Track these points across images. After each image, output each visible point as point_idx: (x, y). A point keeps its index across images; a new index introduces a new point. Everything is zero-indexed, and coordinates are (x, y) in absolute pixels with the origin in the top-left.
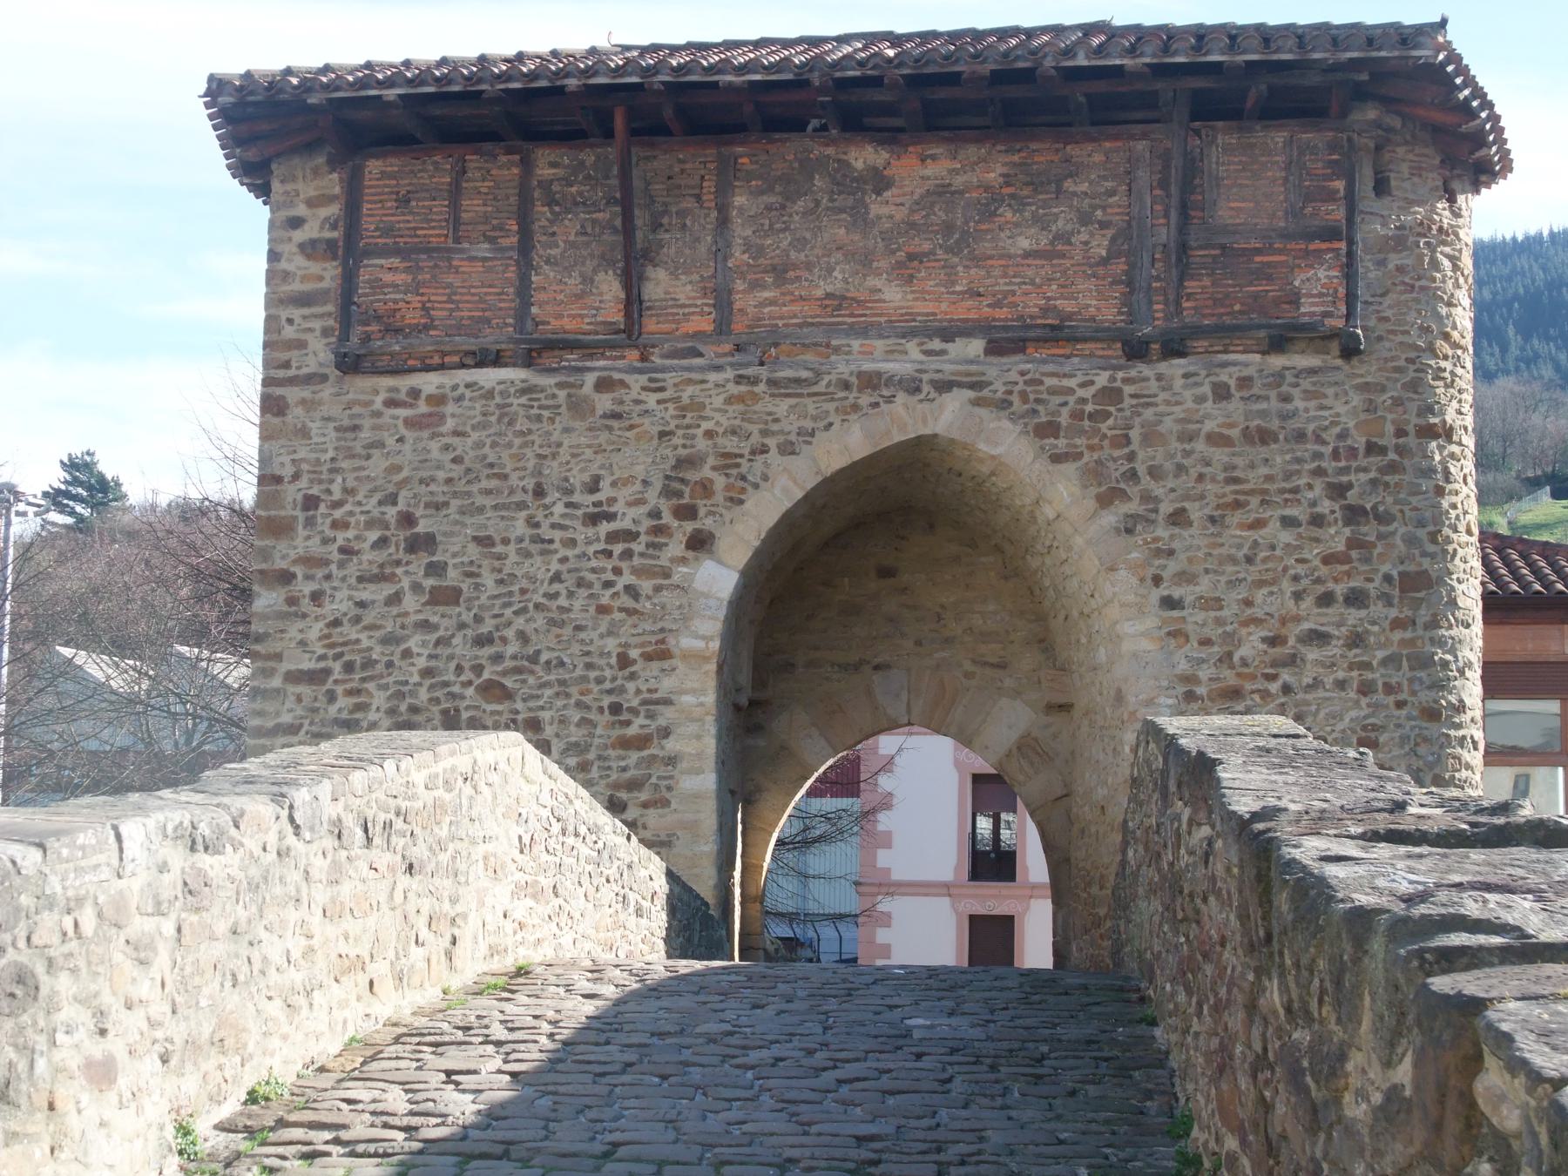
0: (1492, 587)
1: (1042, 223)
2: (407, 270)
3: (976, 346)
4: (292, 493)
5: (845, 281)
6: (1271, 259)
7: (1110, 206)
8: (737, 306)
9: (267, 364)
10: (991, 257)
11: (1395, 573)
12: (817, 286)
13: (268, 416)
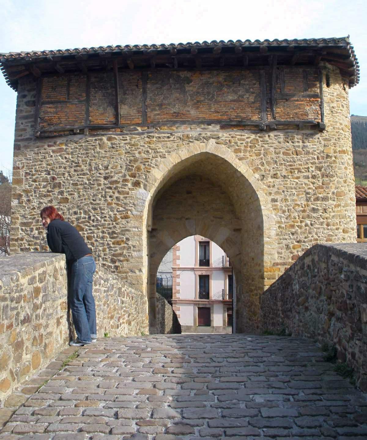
0: (359, 196)
1: (235, 92)
2: (54, 108)
5: (179, 108)
6: (300, 103)
7: (255, 88)
8: (148, 115)
9: (16, 136)
10: (221, 102)
11: (335, 191)
12: (171, 110)
13: (16, 150)
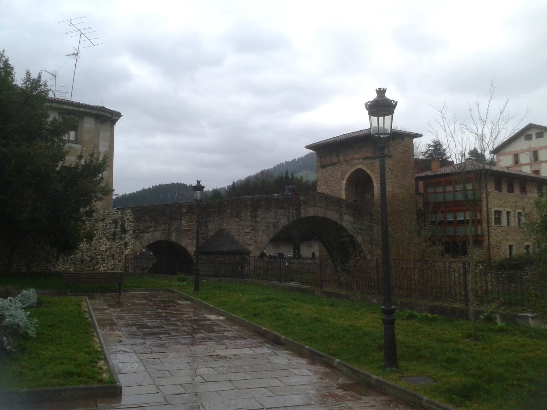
3: (362, 160)
4: (319, 178)
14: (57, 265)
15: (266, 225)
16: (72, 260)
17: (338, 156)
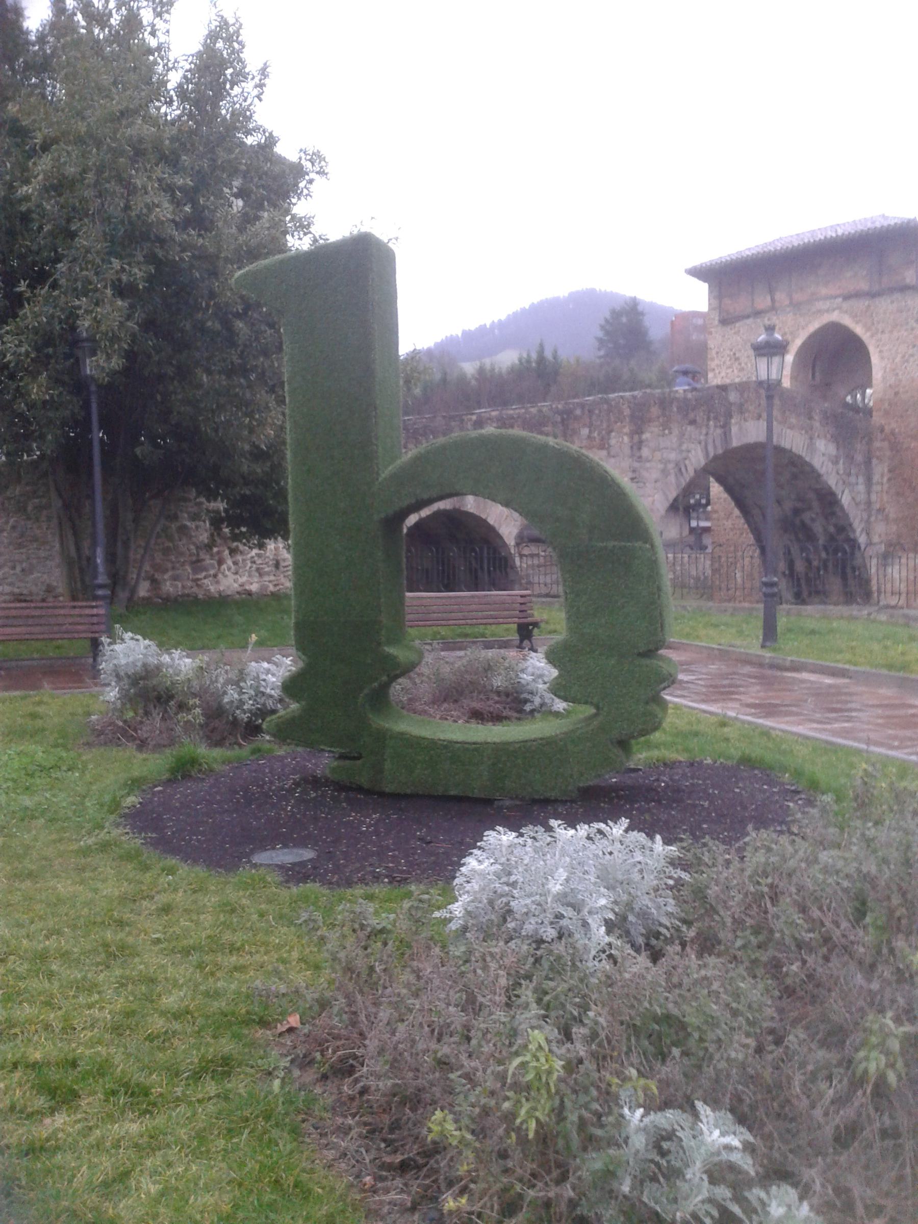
3: (840, 300)
14: (220, 576)
15: (661, 466)
16: (254, 562)
17: (771, 291)
